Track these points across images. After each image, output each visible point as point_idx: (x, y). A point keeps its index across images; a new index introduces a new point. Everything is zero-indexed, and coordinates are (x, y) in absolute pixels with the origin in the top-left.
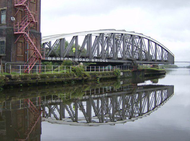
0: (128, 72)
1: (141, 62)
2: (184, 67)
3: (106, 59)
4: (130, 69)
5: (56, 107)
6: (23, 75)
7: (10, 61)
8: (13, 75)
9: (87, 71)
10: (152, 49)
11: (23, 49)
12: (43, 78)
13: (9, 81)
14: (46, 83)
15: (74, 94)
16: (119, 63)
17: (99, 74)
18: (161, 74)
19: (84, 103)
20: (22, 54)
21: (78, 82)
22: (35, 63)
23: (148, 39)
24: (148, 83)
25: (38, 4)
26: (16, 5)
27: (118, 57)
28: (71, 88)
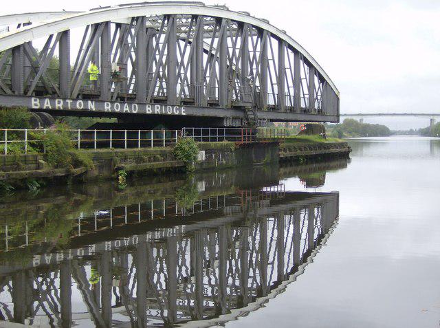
0: (222, 150)
2: (411, 133)
9: (84, 145)
15: (40, 226)
21: (53, 185)
24: (293, 184)
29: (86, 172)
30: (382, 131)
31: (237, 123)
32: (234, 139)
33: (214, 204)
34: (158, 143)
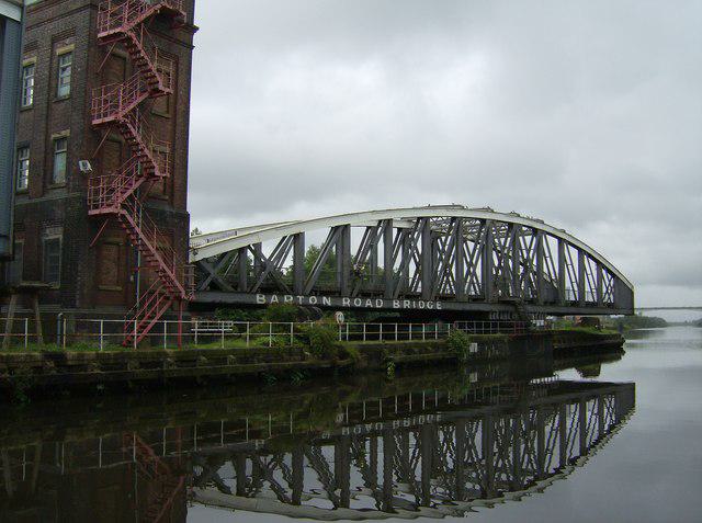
0: (494, 342)
1: (541, 309)
2: (686, 324)
3: (435, 301)
4: (502, 332)
5: (278, 461)
6: (113, 350)
7: (73, 306)
8: (71, 353)
9: (352, 338)
10: (570, 267)
12: (184, 364)
13: (54, 372)
14: (199, 381)
15: (305, 415)
16: (463, 312)
17: (394, 349)
18: (613, 350)
19: (328, 452)
20: (118, 284)
21: (317, 376)
22: (162, 312)
23: (556, 237)
24: (571, 375)
26: (96, 122)
29: (353, 364)
30: (661, 323)
31: (506, 317)
32: (506, 332)
33: (487, 394)
34: (417, 336)
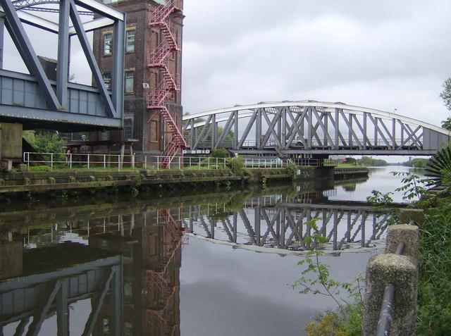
0: (308, 169)
8: (148, 171)
11: (158, 132)
15: (229, 204)
18: (362, 176)
25: (178, 62)
27: (354, 145)
28: (226, 195)
